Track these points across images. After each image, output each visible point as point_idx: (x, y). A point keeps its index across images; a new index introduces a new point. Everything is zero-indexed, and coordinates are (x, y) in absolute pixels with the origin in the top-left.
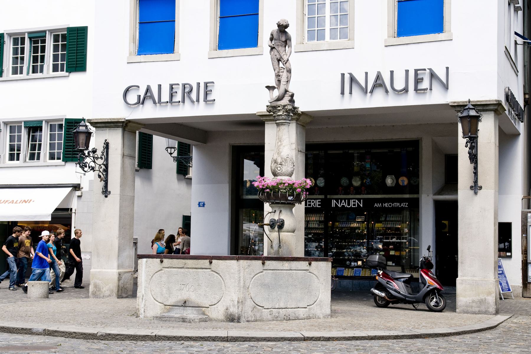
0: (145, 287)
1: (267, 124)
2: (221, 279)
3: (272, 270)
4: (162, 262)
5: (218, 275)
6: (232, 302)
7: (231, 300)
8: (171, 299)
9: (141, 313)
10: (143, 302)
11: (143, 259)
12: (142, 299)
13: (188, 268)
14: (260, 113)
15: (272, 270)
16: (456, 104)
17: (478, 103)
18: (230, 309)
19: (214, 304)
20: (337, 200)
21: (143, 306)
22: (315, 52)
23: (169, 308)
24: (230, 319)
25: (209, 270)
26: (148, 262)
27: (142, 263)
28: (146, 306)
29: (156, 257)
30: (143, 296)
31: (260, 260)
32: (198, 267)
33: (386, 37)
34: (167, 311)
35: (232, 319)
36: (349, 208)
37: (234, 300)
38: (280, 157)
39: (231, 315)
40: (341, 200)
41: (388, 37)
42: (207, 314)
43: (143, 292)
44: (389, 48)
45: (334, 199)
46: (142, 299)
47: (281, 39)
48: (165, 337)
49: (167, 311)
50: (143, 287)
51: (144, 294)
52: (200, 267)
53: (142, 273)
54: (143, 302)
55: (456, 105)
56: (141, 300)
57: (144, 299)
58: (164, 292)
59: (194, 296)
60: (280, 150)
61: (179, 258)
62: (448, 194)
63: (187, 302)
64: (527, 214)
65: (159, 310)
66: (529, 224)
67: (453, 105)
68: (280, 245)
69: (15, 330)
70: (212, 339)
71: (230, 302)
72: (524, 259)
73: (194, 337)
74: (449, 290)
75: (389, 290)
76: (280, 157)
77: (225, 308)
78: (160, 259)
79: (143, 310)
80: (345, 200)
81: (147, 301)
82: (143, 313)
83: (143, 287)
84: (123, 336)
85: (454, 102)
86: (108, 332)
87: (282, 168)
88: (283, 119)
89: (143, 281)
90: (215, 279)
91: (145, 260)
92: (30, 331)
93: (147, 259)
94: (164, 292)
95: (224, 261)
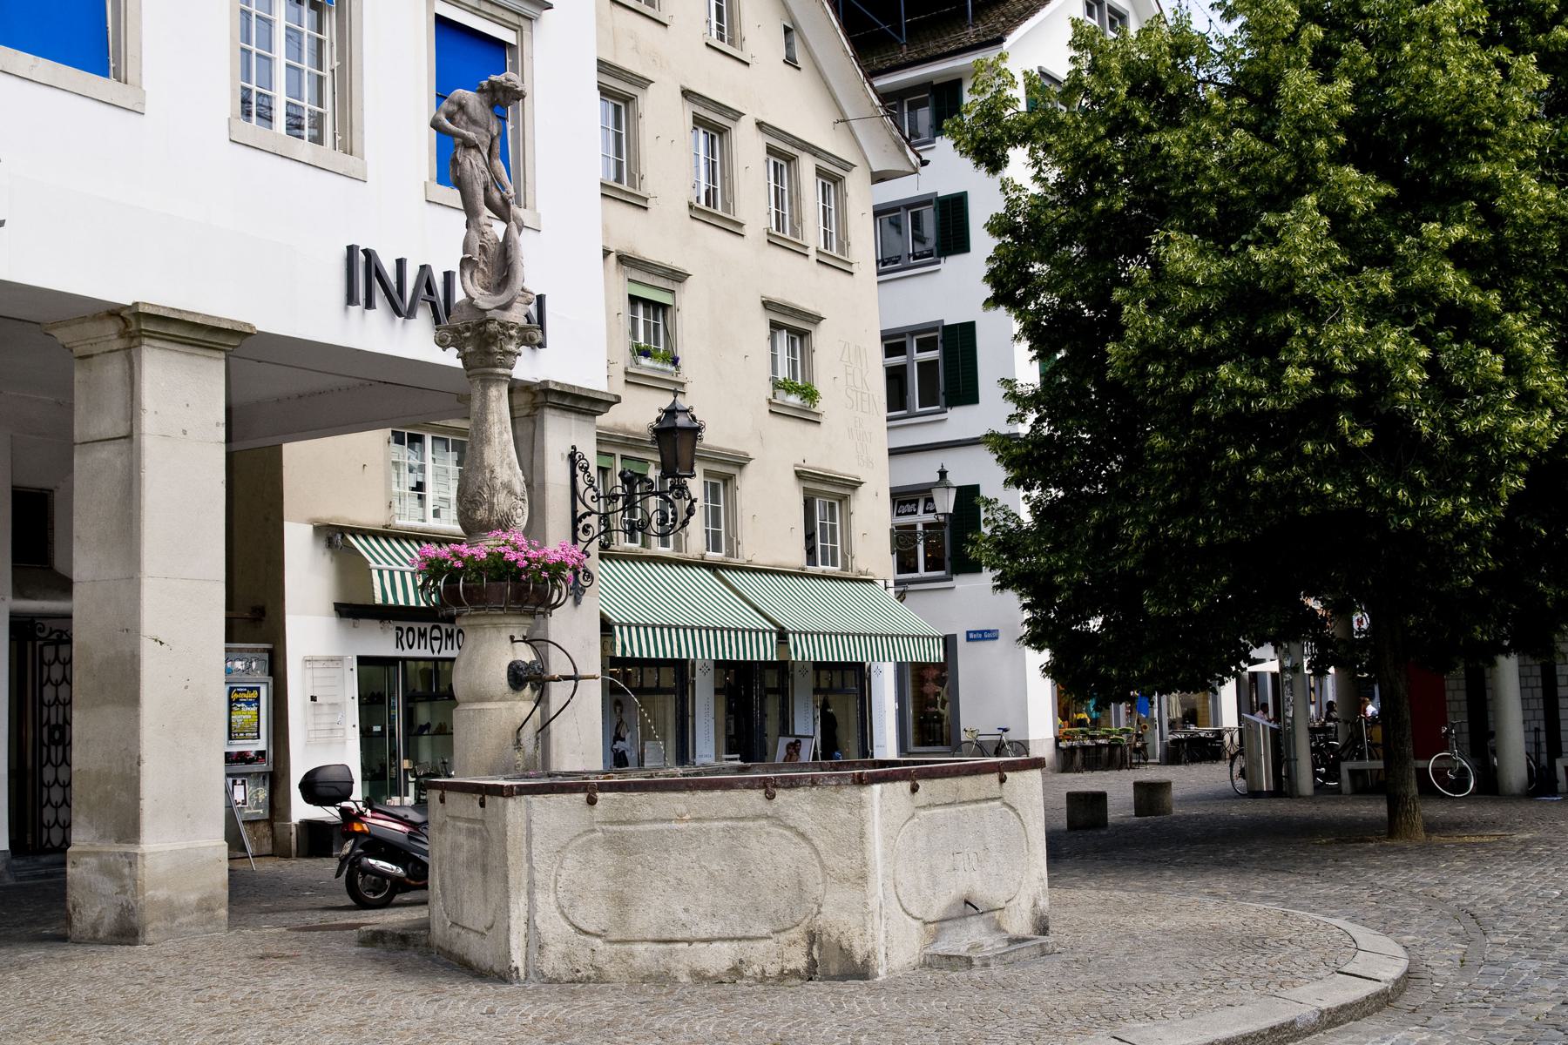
1: (148, 345)
4: (914, 789)
13: (964, 802)
16: (558, 388)
17: (591, 395)
22: (280, 159)
25: (997, 803)
27: (872, 798)
31: (993, 772)
33: (427, 180)
41: (430, 179)
44: (433, 206)
46: (881, 915)
50: (879, 876)
62: (45, 598)
68: (519, 741)
74: (24, 866)
75: (418, 855)
79: (883, 950)
83: (879, 876)
89: (878, 857)
91: (877, 788)
92: (1291, 1031)
94: (924, 882)
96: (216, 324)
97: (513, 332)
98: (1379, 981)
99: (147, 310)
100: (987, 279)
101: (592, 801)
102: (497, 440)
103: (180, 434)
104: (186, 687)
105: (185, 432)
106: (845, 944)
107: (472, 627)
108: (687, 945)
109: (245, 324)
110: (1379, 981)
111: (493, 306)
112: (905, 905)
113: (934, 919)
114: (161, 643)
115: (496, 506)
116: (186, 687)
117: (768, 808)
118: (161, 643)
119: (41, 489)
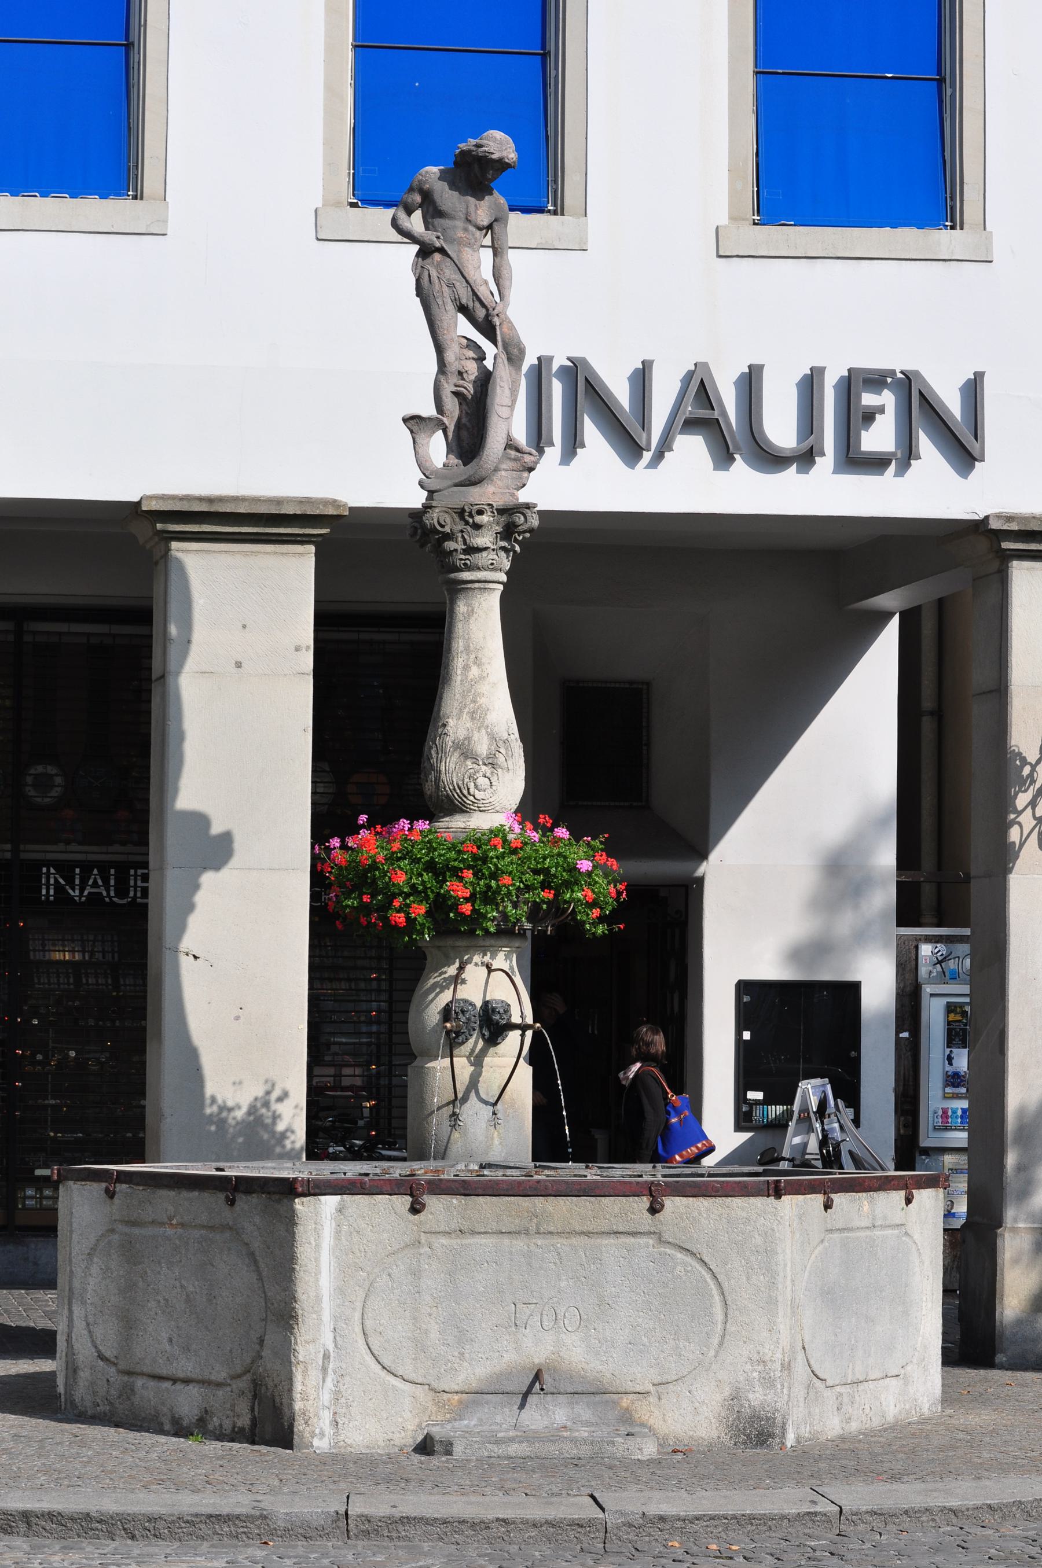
0: (335, 1318)
2: (708, 1277)
3: (841, 1230)
5: (689, 1259)
6: (760, 1368)
7: (756, 1357)
8: (465, 1364)
9: (317, 1431)
10: (329, 1383)
11: (323, 1198)
12: (324, 1370)
14: (161, 502)
15: (841, 1230)
16: (1014, 527)
18: (751, 1396)
19: (676, 1377)
20: (65, 869)
21: (326, 1397)
23: (460, 1402)
24: (748, 1436)
26: (350, 1211)
28: (343, 1400)
29: (387, 1188)
30: (326, 1357)
32: (599, 1229)
33: (723, 220)
34: (448, 1416)
35: (761, 1434)
36: (124, 905)
37: (767, 1358)
38: (483, 732)
39: (755, 1417)
40: (87, 869)
41: (733, 218)
42: (645, 1418)
43: (327, 1339)
45: (49, 864)
46: (324, 1370)
47: (473, 217)
48: (876, 1513)
49: (448, 1416)
50: (326, 1316)
51: (331, 1347)
52: (606, 1229)
53: (317, 1260)
54: (329, 1383)
55: (1016, 528)
56: (314, 1374)
57: (330, 1371)
58: (434, 1335)
59: (579, 1350)
60: (482, 701)
61: (507, 1190)
63: (546, 1377)
64: (917, 948)
65: (407, 1415)
66: (928, 990)
67: (1005, 527)
69: (160, 1525)
70: (1022, 1510)
71: (748, 1367)
72: (902, 1131)
73: (968, 1509)
76: (483, 732)
77: (727, 1392)
78: (104, 1185)
79: (326, 1417)
80: (103, 869)
81: (347, 1379)
82: (329, 1430)
84: (715, 1523)
85: (1010, 518)
86: (654, 1509)
87: (494, 779)
88: (492, 564)
90: (680, 1277)
91: (330, 1202)
93: (345, 1196)
94: (434, 1335)
95: (719, 1200)
96: (274, 510)
97: (484, 519)
98: (603, 1510)
99: (154, 506)
100: (423, 504)
101: (111, 1194)
102: (459, 678)
103: (234, 670)
104: (237, 1018)
105: (239, 665)
106: (277, 1400)
107: (454, 947)
108: (171, 1383)
109: (326, 502)
110: (603, 1510)
111: (450, 483)
112: (386, 1362)
113: (457, 1388)
114: (195, 957)
115: (443, 776)
116: (237, 1018)
117: (227, 1215)
118: (195, 957)
119: (631, 683)
